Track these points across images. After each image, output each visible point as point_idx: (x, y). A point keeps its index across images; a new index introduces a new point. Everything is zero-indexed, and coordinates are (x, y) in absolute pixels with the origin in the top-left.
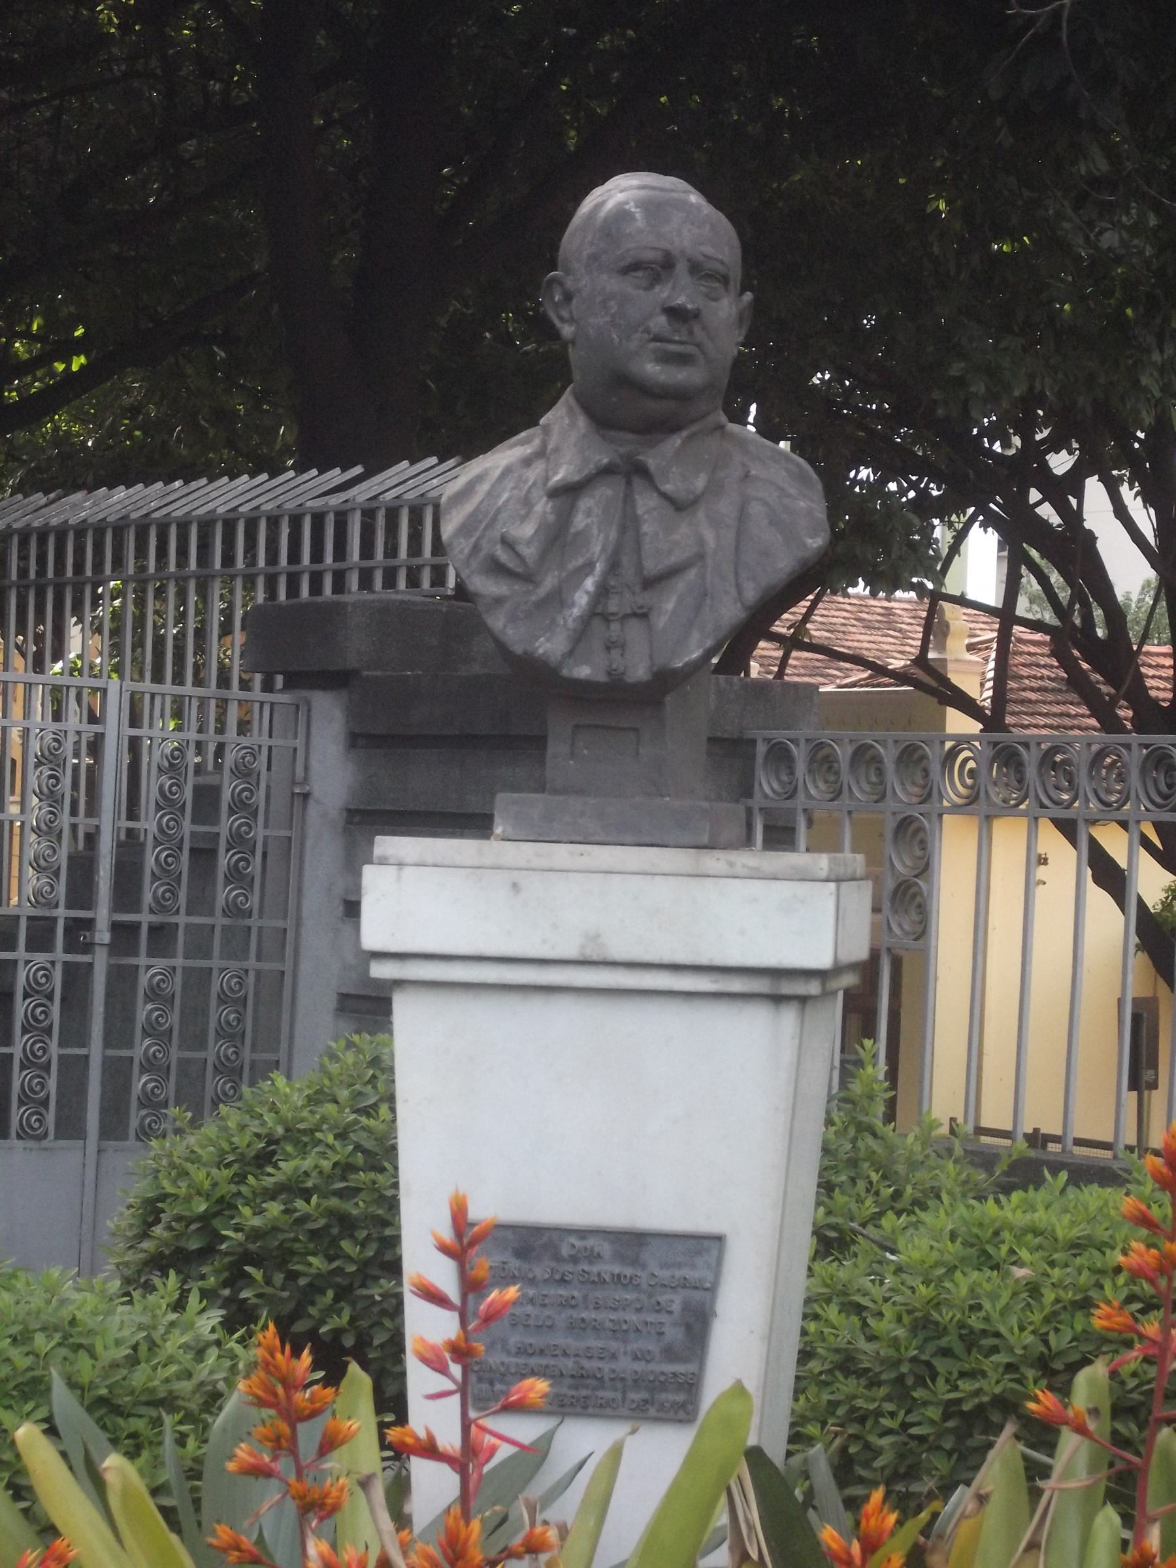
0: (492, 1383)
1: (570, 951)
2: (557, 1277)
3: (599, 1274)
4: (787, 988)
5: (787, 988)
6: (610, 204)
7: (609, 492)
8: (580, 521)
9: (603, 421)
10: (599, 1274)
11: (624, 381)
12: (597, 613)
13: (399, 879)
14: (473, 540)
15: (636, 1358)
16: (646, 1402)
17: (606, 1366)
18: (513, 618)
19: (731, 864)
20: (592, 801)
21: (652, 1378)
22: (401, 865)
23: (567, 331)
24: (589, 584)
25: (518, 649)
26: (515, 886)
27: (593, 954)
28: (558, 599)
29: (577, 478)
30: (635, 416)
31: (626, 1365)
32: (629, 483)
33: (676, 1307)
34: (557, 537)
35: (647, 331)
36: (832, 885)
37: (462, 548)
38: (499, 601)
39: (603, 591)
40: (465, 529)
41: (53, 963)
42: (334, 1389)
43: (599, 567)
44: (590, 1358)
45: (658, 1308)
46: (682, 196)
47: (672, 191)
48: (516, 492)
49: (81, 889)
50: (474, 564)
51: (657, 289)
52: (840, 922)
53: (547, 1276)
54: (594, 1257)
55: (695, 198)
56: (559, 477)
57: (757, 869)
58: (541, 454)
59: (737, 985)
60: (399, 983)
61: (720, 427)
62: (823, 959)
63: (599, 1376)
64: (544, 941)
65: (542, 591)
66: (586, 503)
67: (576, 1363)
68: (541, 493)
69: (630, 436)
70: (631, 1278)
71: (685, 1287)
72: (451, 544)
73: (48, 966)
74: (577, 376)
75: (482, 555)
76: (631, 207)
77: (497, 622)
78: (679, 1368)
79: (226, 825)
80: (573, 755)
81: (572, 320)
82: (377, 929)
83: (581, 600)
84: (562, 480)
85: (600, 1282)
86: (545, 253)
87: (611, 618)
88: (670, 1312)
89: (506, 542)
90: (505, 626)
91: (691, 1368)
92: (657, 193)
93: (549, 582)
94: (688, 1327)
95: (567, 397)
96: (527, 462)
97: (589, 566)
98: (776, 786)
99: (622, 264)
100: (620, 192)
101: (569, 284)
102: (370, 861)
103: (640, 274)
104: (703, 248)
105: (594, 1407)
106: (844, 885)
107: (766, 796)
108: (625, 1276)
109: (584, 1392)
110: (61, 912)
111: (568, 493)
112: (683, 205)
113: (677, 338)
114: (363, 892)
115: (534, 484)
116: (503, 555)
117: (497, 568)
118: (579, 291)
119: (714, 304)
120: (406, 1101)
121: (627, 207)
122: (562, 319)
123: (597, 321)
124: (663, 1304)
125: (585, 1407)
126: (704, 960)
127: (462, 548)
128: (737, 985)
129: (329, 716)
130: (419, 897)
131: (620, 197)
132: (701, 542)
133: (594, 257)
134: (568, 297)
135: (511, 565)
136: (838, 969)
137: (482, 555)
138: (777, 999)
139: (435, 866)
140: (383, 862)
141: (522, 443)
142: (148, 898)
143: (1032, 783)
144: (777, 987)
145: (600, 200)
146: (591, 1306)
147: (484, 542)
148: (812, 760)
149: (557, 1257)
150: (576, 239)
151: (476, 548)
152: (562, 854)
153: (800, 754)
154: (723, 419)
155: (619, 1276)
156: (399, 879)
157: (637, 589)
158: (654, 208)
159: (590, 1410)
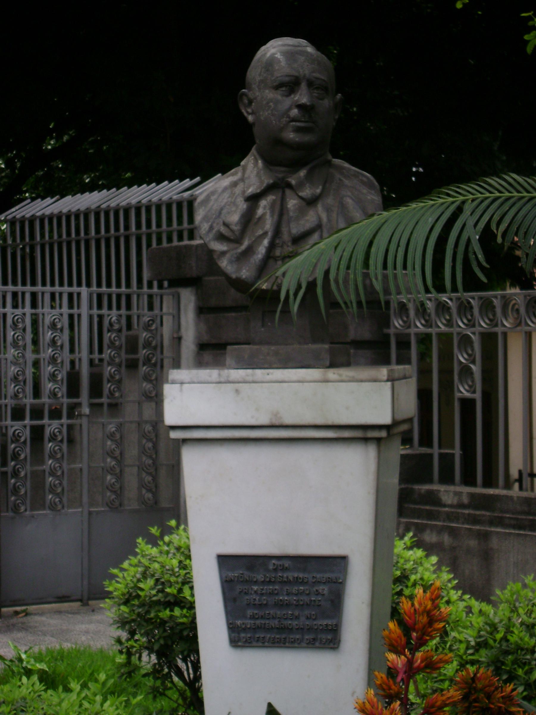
0: (239, 633)
1: (264, 420)
2: (268, 580)
3: (287, 577)
4: (371, 434)
5: (371, 434)
6: (268, 55)
7: (274, 197)
8: (260, 212)
9: (270, 162)
10: (287, 577)
11: (278, 142)
12: (269, 256)
13: (181, 390)
14: (210, 223)
15: (307, 618)
16: (314, 639)
17: (295, 623)
18: (231, 262)
19: (340, 375)
20: (273, 348)
21: (316, 628)
22: (182, 383)
23: (250, 118)
24: (266, 242)
25: (234, 276)
26: (237, 391)
27: (277, 423)
28: (249, 251)
29: (258, 191)
30: (285, 159)
31: (303, 622)
32: (284, 193)
33: (326, 592)
34: (248, 219)
35: (288, 117)
36: (389, 383)
37: (205, 227)
38: (223, 253)
39: (272, 246)
40: (205, 218)
41: (62, 425)
42: (455, 592)
43: (270, 234)
44: (286, 619)
45: (318, 593)
46: (303, 49)
47: (299, 46)
48: (230, 199)
49: (73, 390)
50: (211, 235)
51: (292, 96)
52: (395, 401)
53: (263, 579)
54: (284, 569)
55: (310, 49)
56: (251, 191)
57: (353, 377)
58: (242, 180)
59: (346, 434)
60: (185, 441)
61: (329, 162)
62: (387, 420)
63: (290, 628)
64: (253, 417)
65: (243, 247)
66: (263, 203)
67: (279, 621)
68: (242, 199)
69: (283, 169)
70: (303, 579)
71: (329, 582)
72: (200, 226)
73: (60, 427)
74: (257, 141)
75: (214, 231)
76: (278, 56)
77: (224, 264)
78: (329, 622)
79: (143, 353)
80: (263, 326)
81: (252, 113)
82: (172, 414)
83: (262, 250)
84: (251, 192)
85: (288, 582)
86: (241, 81)
87: (277, 259)
88: (323, 595)
89: (225, 224)
90: (227, 266)
91: (334, 622)
92: (290, 48)
93: (246, 243)
94: (332, 601)
95: (254, 150)
96: (235, 184)
97: (266, 233)
98: (401, 322)
99: (275, 84)
100: (275, 49)
101: (251, 95)
102: (167, 382)
103: (284, 89)
104: (315, 75)
105: (289, 642)
106: (396, 383)
107: (396, 328)
108: (300, 578)
109: (284, 636)
110: (66, 401)
111: (253, 200)
112: (303, 53)
113: (303, 120)
114: (164, 397)
115: (239, 194)
116: (223, 229)
117: (221, 237)
118: (256, 98)
119: (321, 101)
120: (191, 497)
121: (276, 56)
122: (248, 113)
123: (264, 114)
124: (320, 591)
125: (284, 643)
126: (330, 423)
127: (205, 227)
128: (346, 434)
129: (188, 298)
130: (191, 398)
131: (273, 51)
132: (320, 219)
133: (261, 81)
134: (250, 102)
135: (226, 234)
136: (395, 423)
137: (214, 231)
138: (366, 440)
139: (199, 383)
140: (173, 382)
141: (233, 175)
142: (106, 392)
143: (523, 316)
144: (362, 434)
145: (263, 53)
146: (285, 593)
147: (215, 225)
148: (417, 311)
149: (268, 570)
150: (254, 73)
151: (211, 228)
152: (259, 373)
153: (411, 307)
154: (330, 157)
155: (297, 578)
156: (181, 390)
157: (290, 244)
158: (291, 55)
159: (287, 644)
